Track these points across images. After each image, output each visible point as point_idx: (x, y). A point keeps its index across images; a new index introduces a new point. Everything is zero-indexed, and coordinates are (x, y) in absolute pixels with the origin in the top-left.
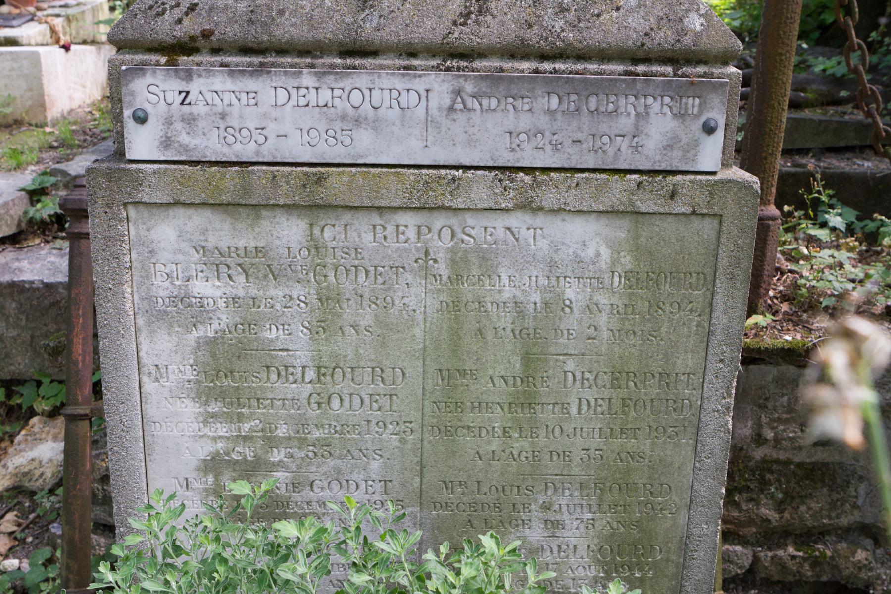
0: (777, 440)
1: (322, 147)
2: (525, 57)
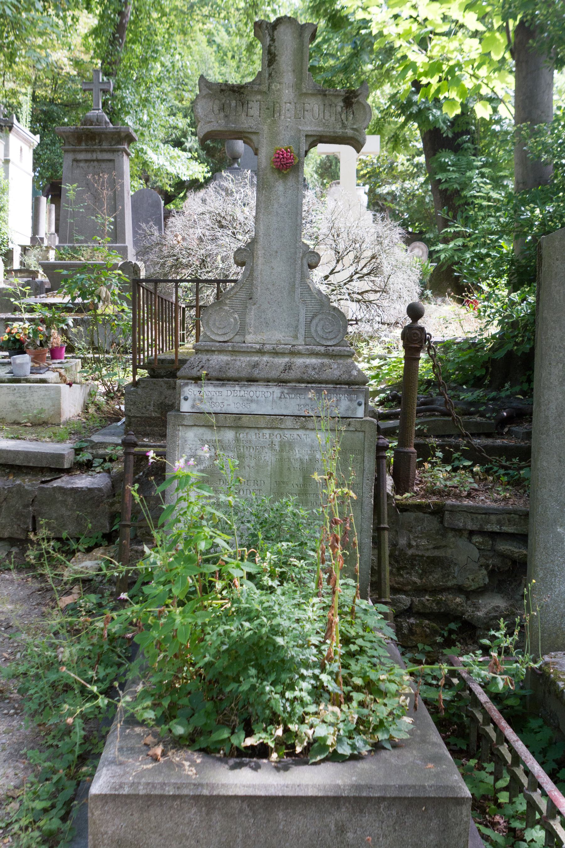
0: (417, 546)
1: (241, 409)
2: (303, 383)
